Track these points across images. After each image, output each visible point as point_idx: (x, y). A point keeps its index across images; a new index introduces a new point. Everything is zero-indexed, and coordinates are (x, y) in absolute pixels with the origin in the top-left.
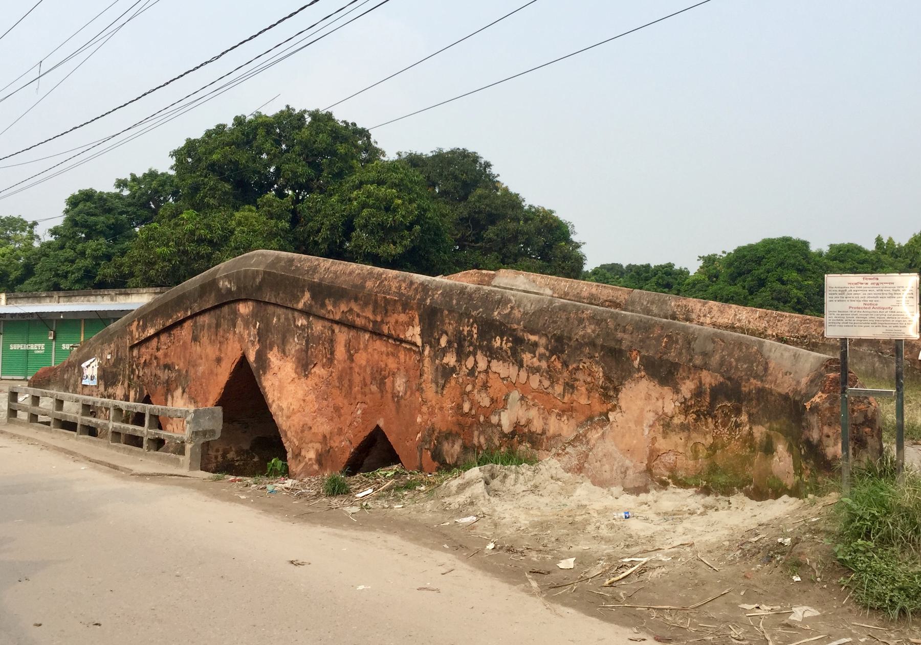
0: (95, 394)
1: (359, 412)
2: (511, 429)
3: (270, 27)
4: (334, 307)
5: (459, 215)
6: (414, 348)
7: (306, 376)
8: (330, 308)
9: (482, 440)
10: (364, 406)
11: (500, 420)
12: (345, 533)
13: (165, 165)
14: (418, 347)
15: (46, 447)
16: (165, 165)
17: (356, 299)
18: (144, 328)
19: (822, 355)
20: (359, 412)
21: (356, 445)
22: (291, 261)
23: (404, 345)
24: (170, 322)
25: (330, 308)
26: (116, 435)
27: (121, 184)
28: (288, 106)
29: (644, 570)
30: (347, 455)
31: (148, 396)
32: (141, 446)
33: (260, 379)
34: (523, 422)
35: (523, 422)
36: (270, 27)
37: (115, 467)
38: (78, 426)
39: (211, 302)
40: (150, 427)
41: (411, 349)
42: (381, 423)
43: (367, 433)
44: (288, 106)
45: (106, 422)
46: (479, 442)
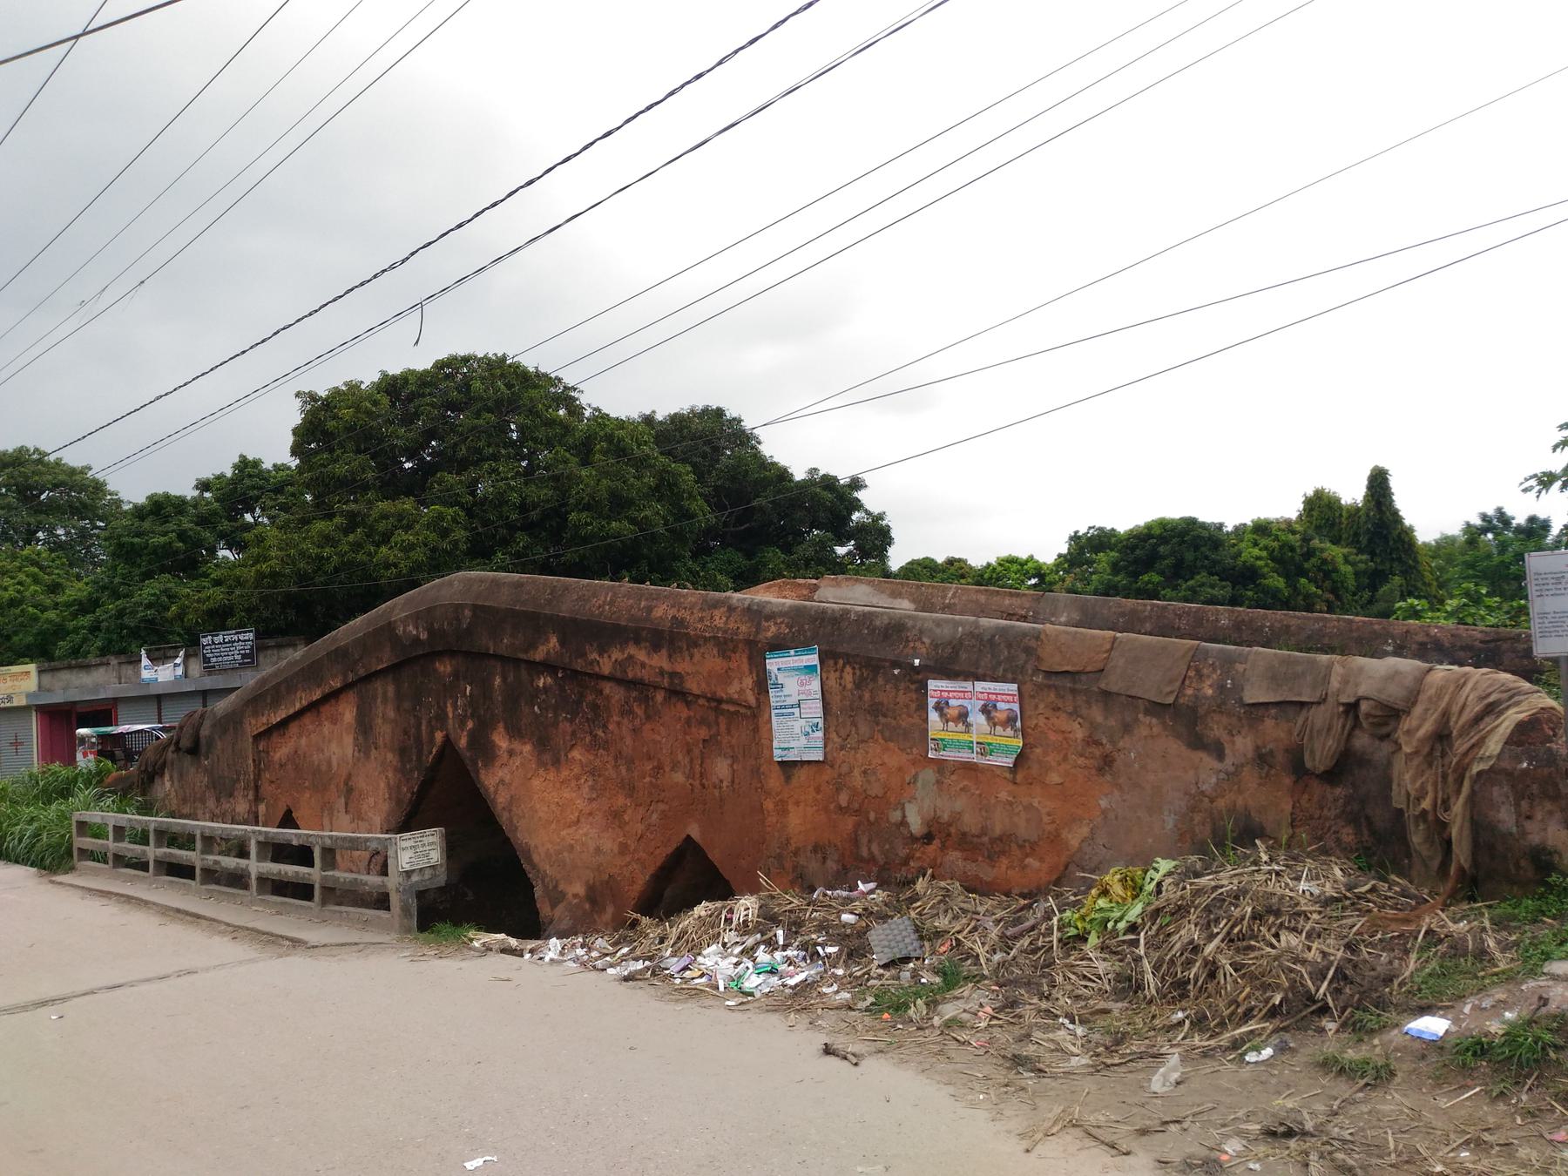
1: (655, 816)
2: (925, 831)
3: (649, 108)
4: (601, 655)
5: (730, 510)
6: (742, 710)
7: (556, 762)
8: (595, 656)
9: (875, 848)
10: (662, 806)
11: (904, 816)
14: (750, 707)
15: (236, 931)
17: (637, 641)
18: (1330, 666)
21: (652, 870)
22: (519, 585)
23: (725, 706)
24: (317, 695)
25: (595, 656)
26: (262, 880)
27: (204, 486)
29: (37, 835)
31: (289, 812)
34: (946, 817)
35: (946, 817)
36: (649, 108)
37: (198, 916)
38: (198, 871)
39: (385, 659)
42: (694, 831)
43: (670, 850)
45: (243, 862)
46: (871, 853)
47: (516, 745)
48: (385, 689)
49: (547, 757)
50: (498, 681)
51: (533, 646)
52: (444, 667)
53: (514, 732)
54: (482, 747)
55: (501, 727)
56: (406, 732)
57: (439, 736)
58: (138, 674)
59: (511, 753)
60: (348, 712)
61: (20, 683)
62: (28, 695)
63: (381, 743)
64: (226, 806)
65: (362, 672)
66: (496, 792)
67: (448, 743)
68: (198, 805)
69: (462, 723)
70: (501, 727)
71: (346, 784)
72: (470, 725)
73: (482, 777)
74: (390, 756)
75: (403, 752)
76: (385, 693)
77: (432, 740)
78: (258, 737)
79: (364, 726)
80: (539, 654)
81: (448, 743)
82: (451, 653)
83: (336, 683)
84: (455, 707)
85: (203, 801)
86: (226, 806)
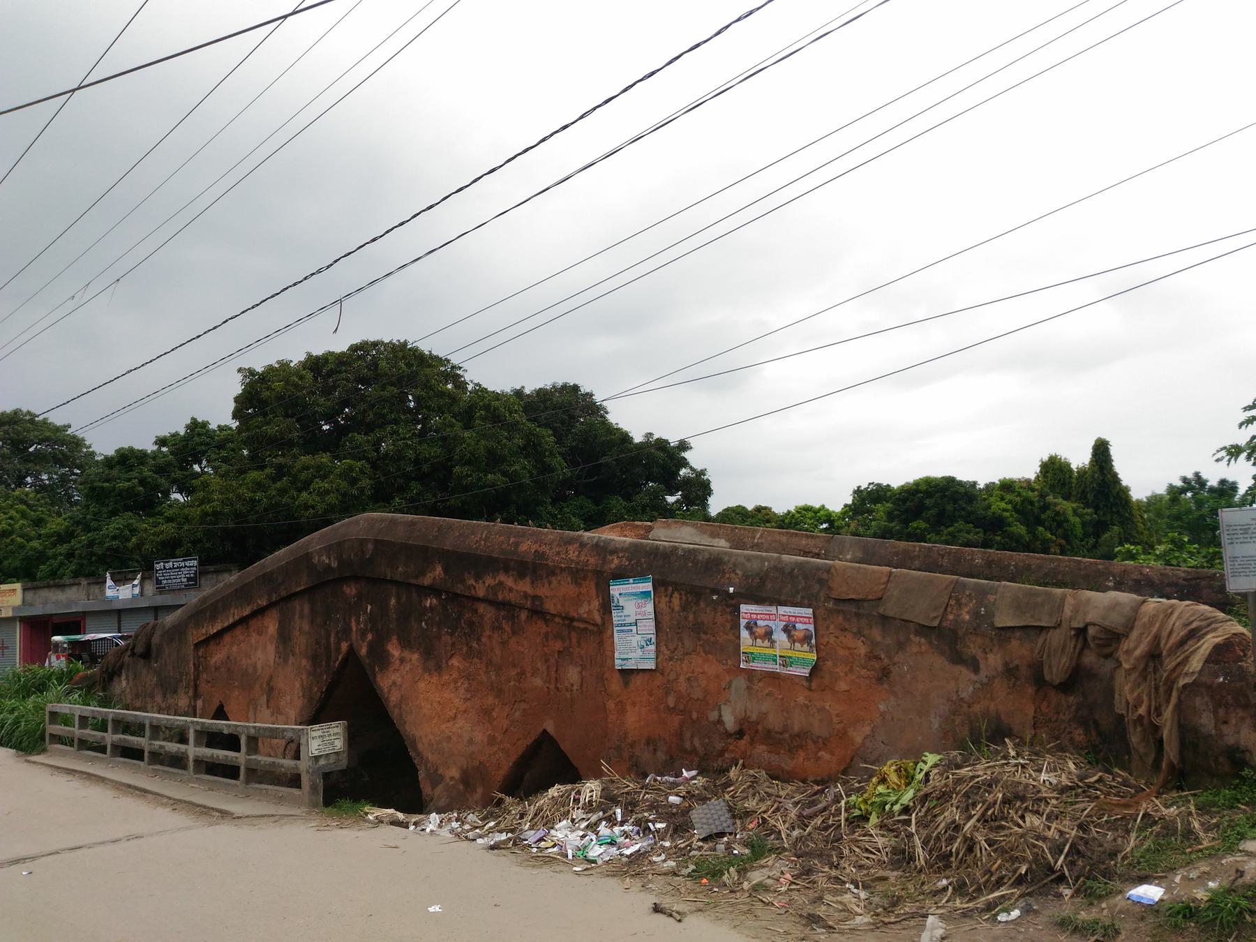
0: (149, 706)
1: (518, 714)
2: (737, 728)
6: (590, 627)
8: (472, 582)
9: (697, 742)
10: (523, 706)
11: (720, 716)
12: (237, 808)
13: (220, 413)
15: (177, 804)
16: (220, 413)
17: (507, 570)
19: (1134, 596)
20: (518, 714)
21: (513, 759)
22: (412, 524)
24: (247, 611)
25: (472, 582)
27: (161, 442)
28: (1101, 451)
30: (503, 772)
32: (184, 767)
33: (375, 676)
38: (146, 754)
39: (303, 583)
40: (248, 753)
41: (586, 629)
42: (550, 726)
43: (529, 741)
44: (1101, 451)
47: (407, 654)
48: (302, 608)
49: (431, 663)
50: (393, 601)
51: (422, 573)
52: (350, 590)
53: (406, 644)
54: (380, 657)
55: (394, 640)
56: (318, 643)
57: (344, 646)
58: (103, 592)
59: (402, 660)
60: (271, 625)
61: (3, 599)
62: (14, 609)
63: (297, 651)
64: (171, 701)
65: (284, 594)
66: (389, 692)
67: (352, 651)
68: (148, 700)
69: (363, 634)
70: (394, 640)
71: (268, 684)
72: (370, 637)
73: (379, 676)
74: (304, 662)
75: (314, 659)
76: (302, 611)
77: (338, 650)
78: (197, 645)
79: (284, 637)
80: (427, 581)
81: (352, 651)
82: (355, 578)
83: (263, 602)
84: (358, 623)
85: (152, 697)
86: (171, 701)
